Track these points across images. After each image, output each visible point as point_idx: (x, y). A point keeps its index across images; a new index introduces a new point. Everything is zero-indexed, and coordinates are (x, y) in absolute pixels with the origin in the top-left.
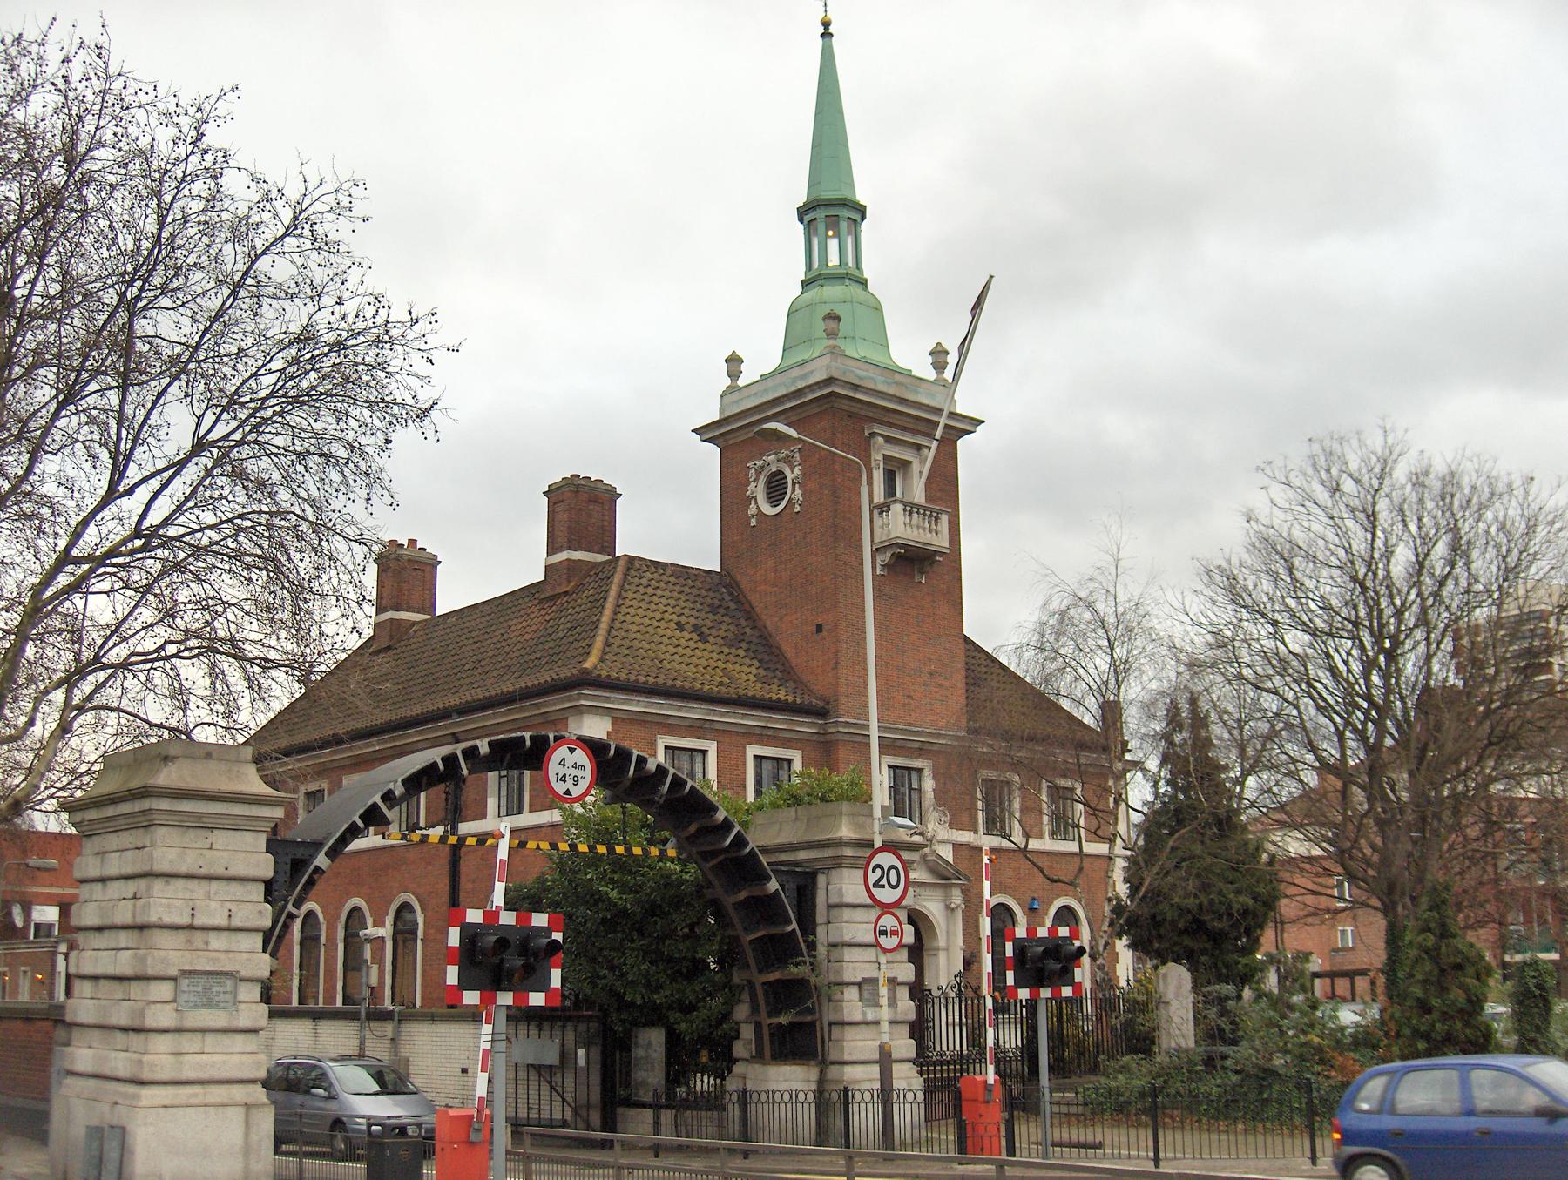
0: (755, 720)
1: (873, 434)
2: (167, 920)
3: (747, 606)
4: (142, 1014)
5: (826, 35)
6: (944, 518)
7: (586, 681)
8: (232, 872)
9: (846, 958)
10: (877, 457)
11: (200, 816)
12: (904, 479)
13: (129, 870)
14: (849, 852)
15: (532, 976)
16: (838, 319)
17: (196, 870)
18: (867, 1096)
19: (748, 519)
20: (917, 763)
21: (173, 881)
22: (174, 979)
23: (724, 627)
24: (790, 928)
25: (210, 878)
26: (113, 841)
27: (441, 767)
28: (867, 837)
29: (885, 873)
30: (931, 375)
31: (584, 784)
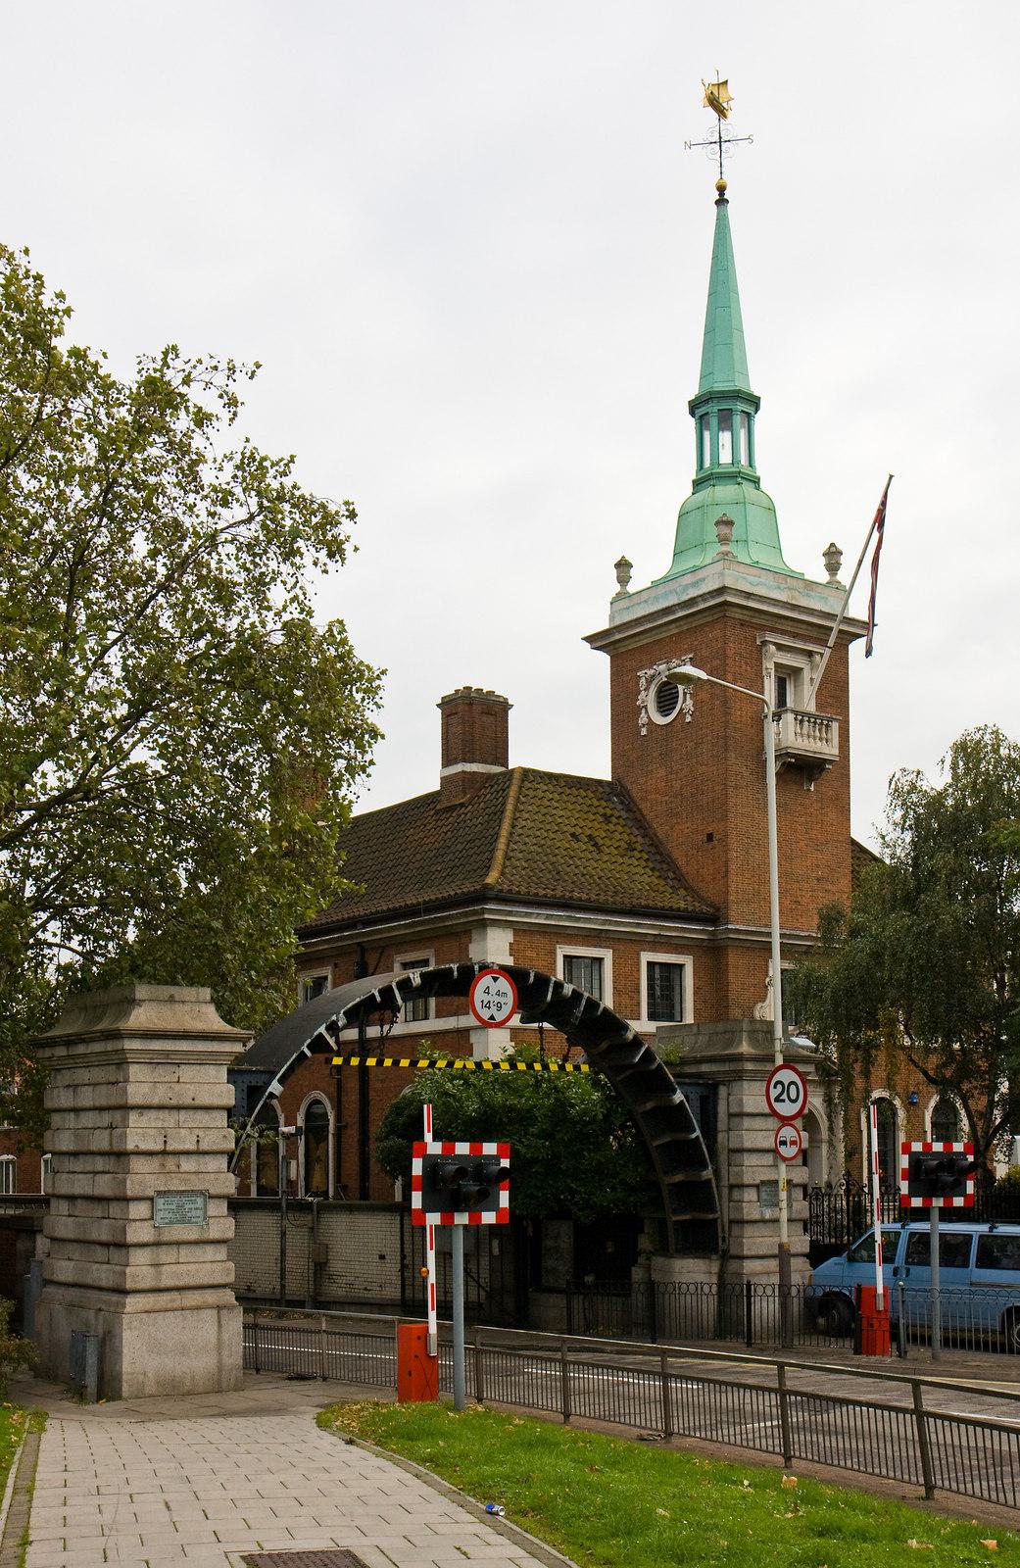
0: (647, 927)
1: (764, 643)
2: (143, 1147)
3: (639, 817)
4: (124, 1231)
5: (721, 202)
6: (835, 726)
7: (483, 896)
8: (198, 1102)
9: (746, 1163)
10: (769, 665)
11: (167, 1053)
12: (795, 681)
13: (104, 1102)
14: (749, 1066)
15: (486, 1199)
16: (730, 523)
17: (166, 1102)
18: (769, 1292)
19: (638, 729)
21: (146, 1112)
22: (151, 1199)
23: (617, 836)
24: (694, 1136)
25: (178, 1108)
26: (84, 1075)
27: (379, 999)
29: (786, 1089)
30: (823, 577)
31: (507, 1010)
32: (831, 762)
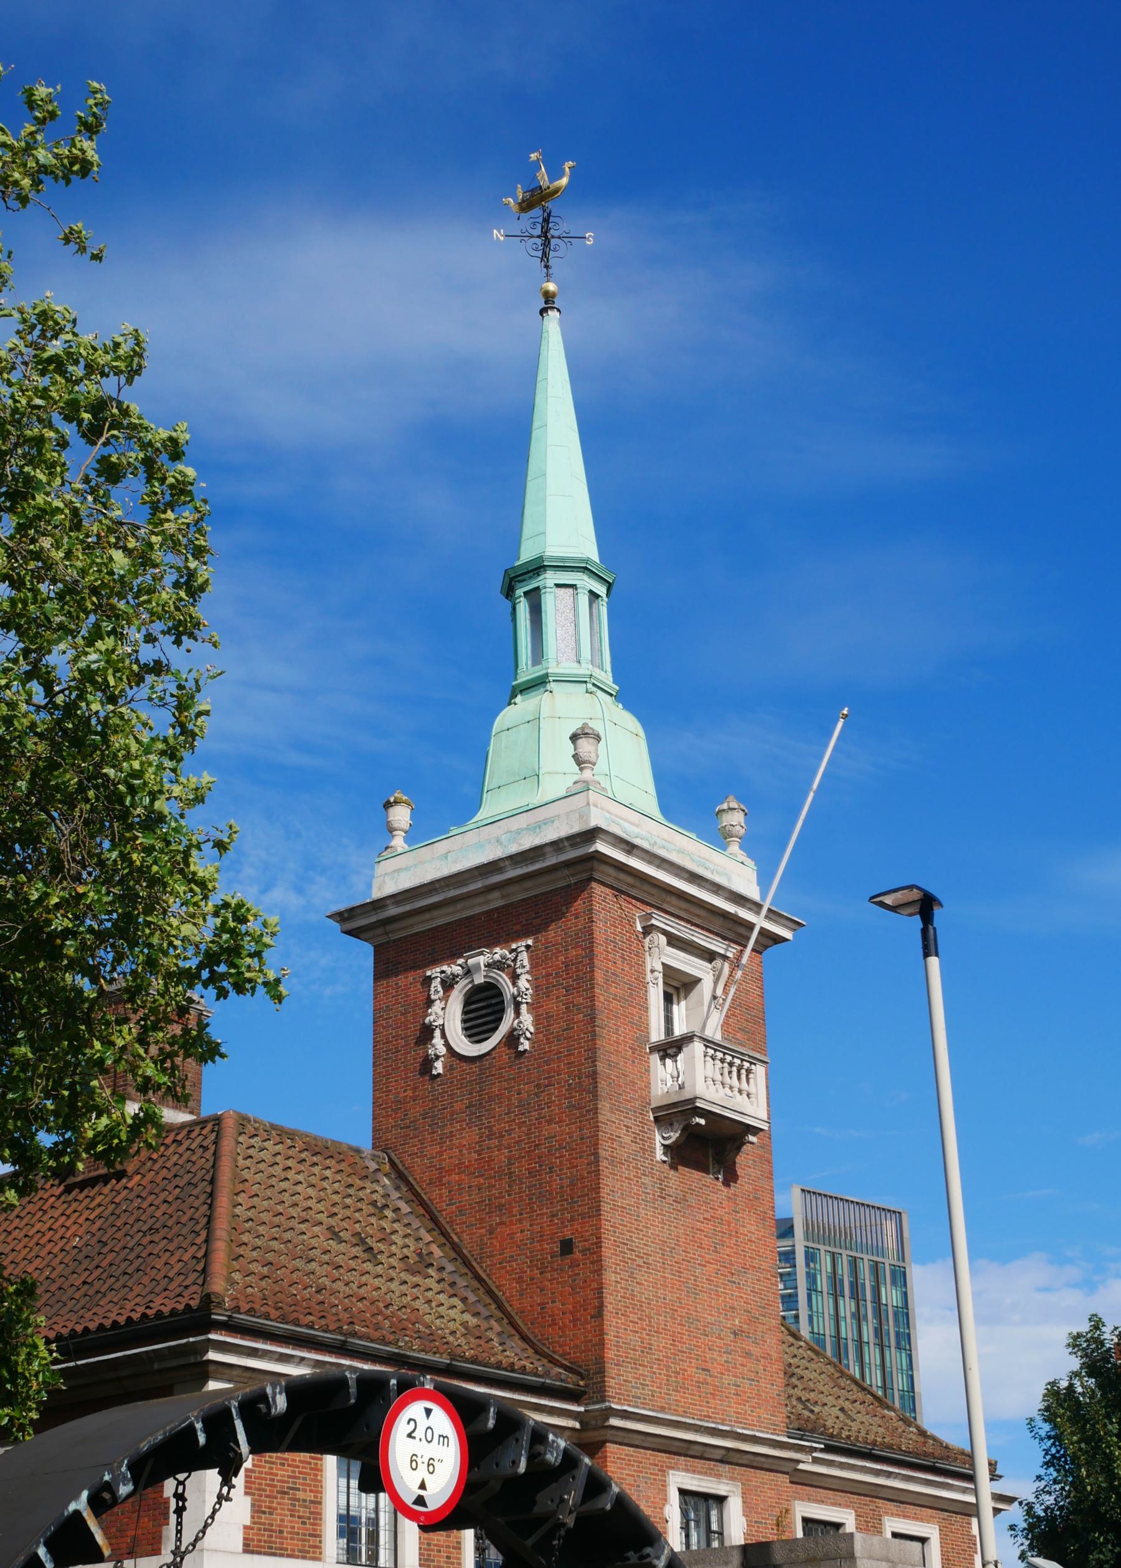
1: (648, 930)
20: (720, 1489)
28: (426, 1535)
32: (756, 1131)
